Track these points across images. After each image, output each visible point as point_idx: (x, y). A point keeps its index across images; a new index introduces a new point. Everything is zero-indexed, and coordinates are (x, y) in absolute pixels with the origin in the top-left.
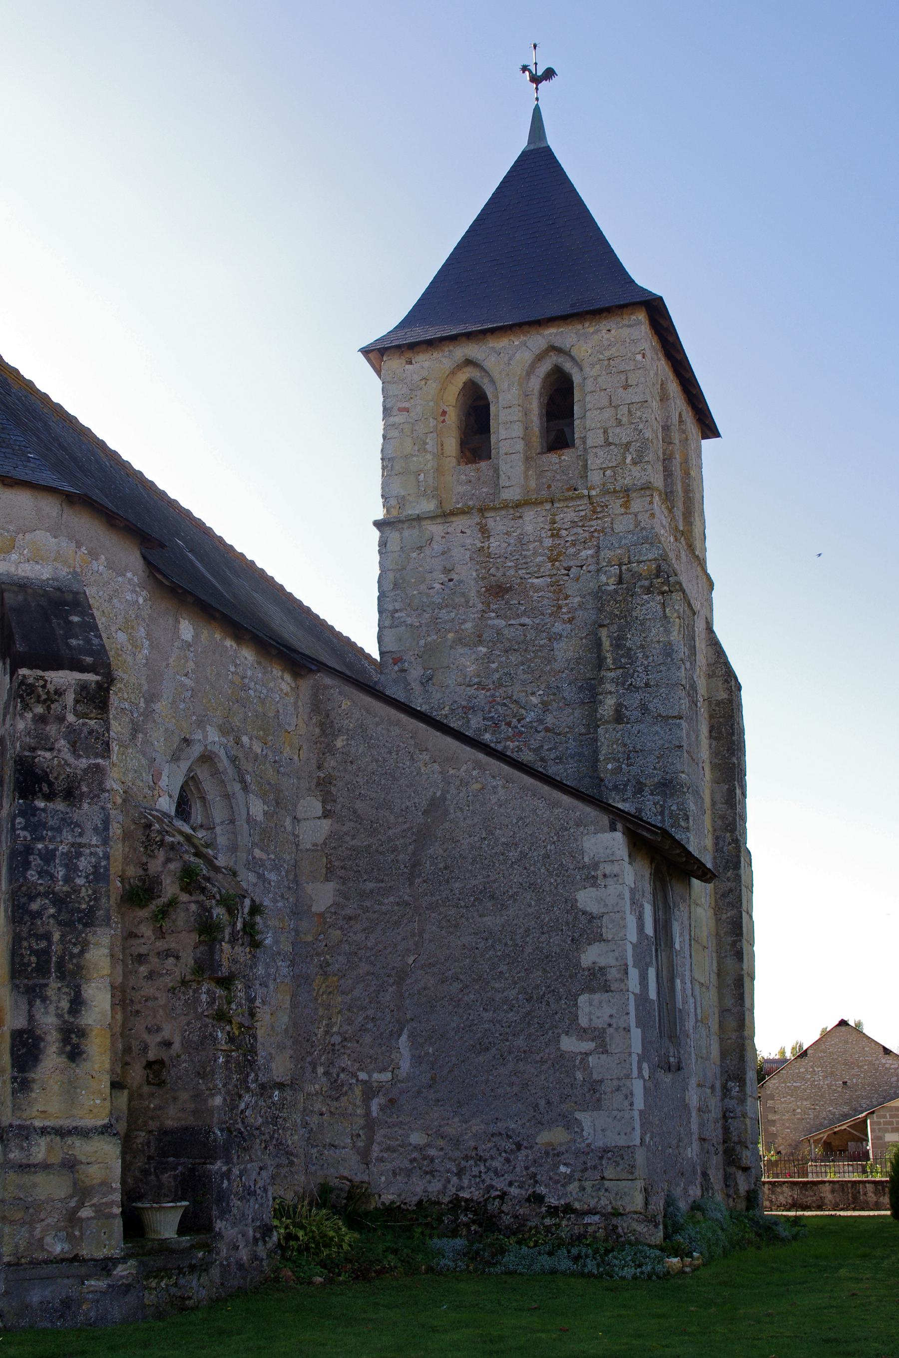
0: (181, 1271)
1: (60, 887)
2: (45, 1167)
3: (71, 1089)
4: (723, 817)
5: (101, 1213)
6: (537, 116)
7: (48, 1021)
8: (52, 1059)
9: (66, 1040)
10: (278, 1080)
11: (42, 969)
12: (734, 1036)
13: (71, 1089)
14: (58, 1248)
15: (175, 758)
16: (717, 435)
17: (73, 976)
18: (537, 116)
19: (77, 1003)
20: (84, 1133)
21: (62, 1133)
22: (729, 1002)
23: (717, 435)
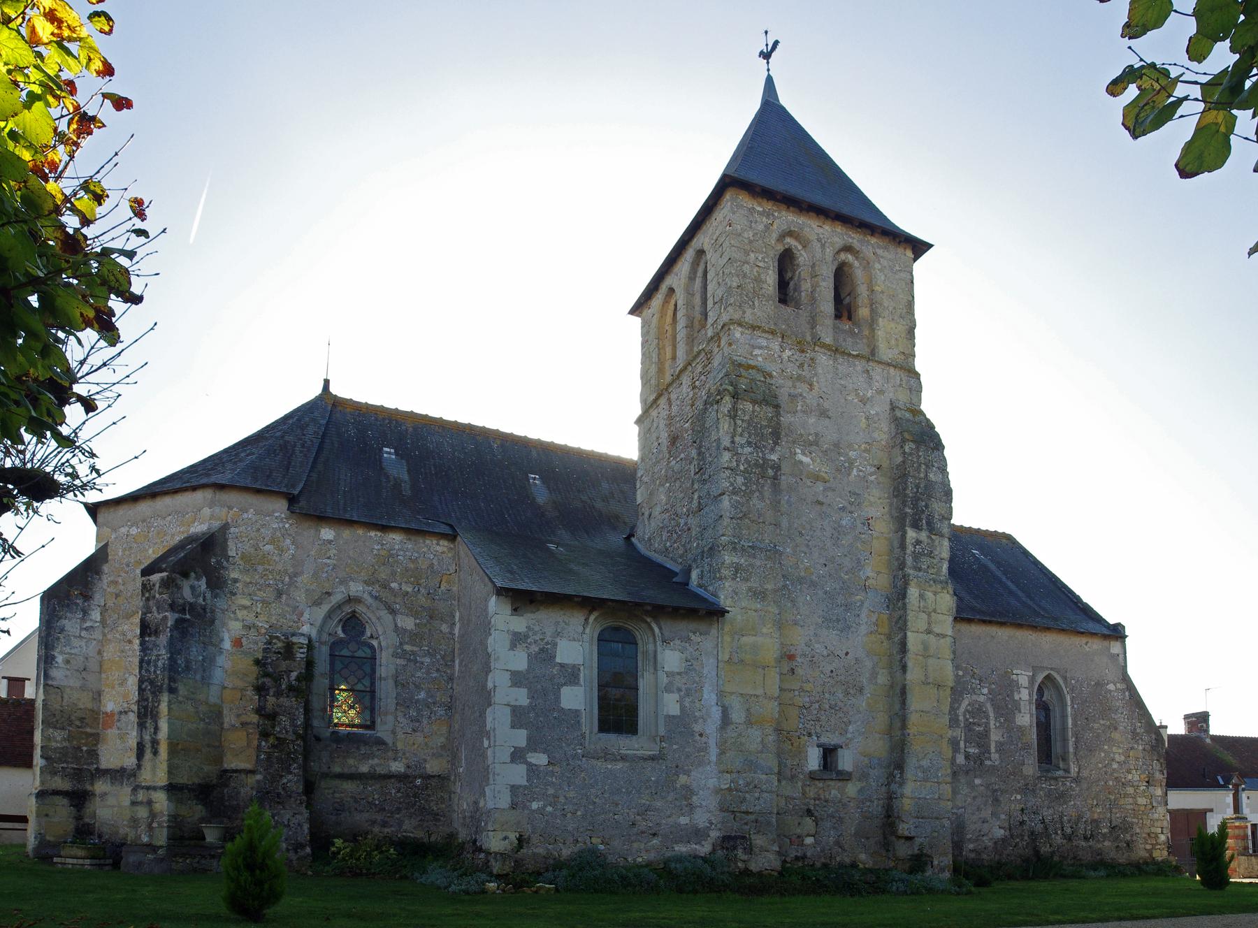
0: (203, 857)
1: (152, 676)
2: (141, 803)
3: (154, 768)
4: (898, 559)
5: (160, 826)
6: (769, 82)
7: (147, 738)
8: (148, 755)
9: (153, 747)
10: (990, 829)
11: (145, 715)
12: (899, 733)
13: (154, 768)
14: (145, 839)
15: (317, 603)
16: (928, 246)
17: (155, 717)
18: (769, 82)
19: (156, 729)
20: (155, 788)
21: (148, 788)
22: (897, 707)
23: (928, 246)
